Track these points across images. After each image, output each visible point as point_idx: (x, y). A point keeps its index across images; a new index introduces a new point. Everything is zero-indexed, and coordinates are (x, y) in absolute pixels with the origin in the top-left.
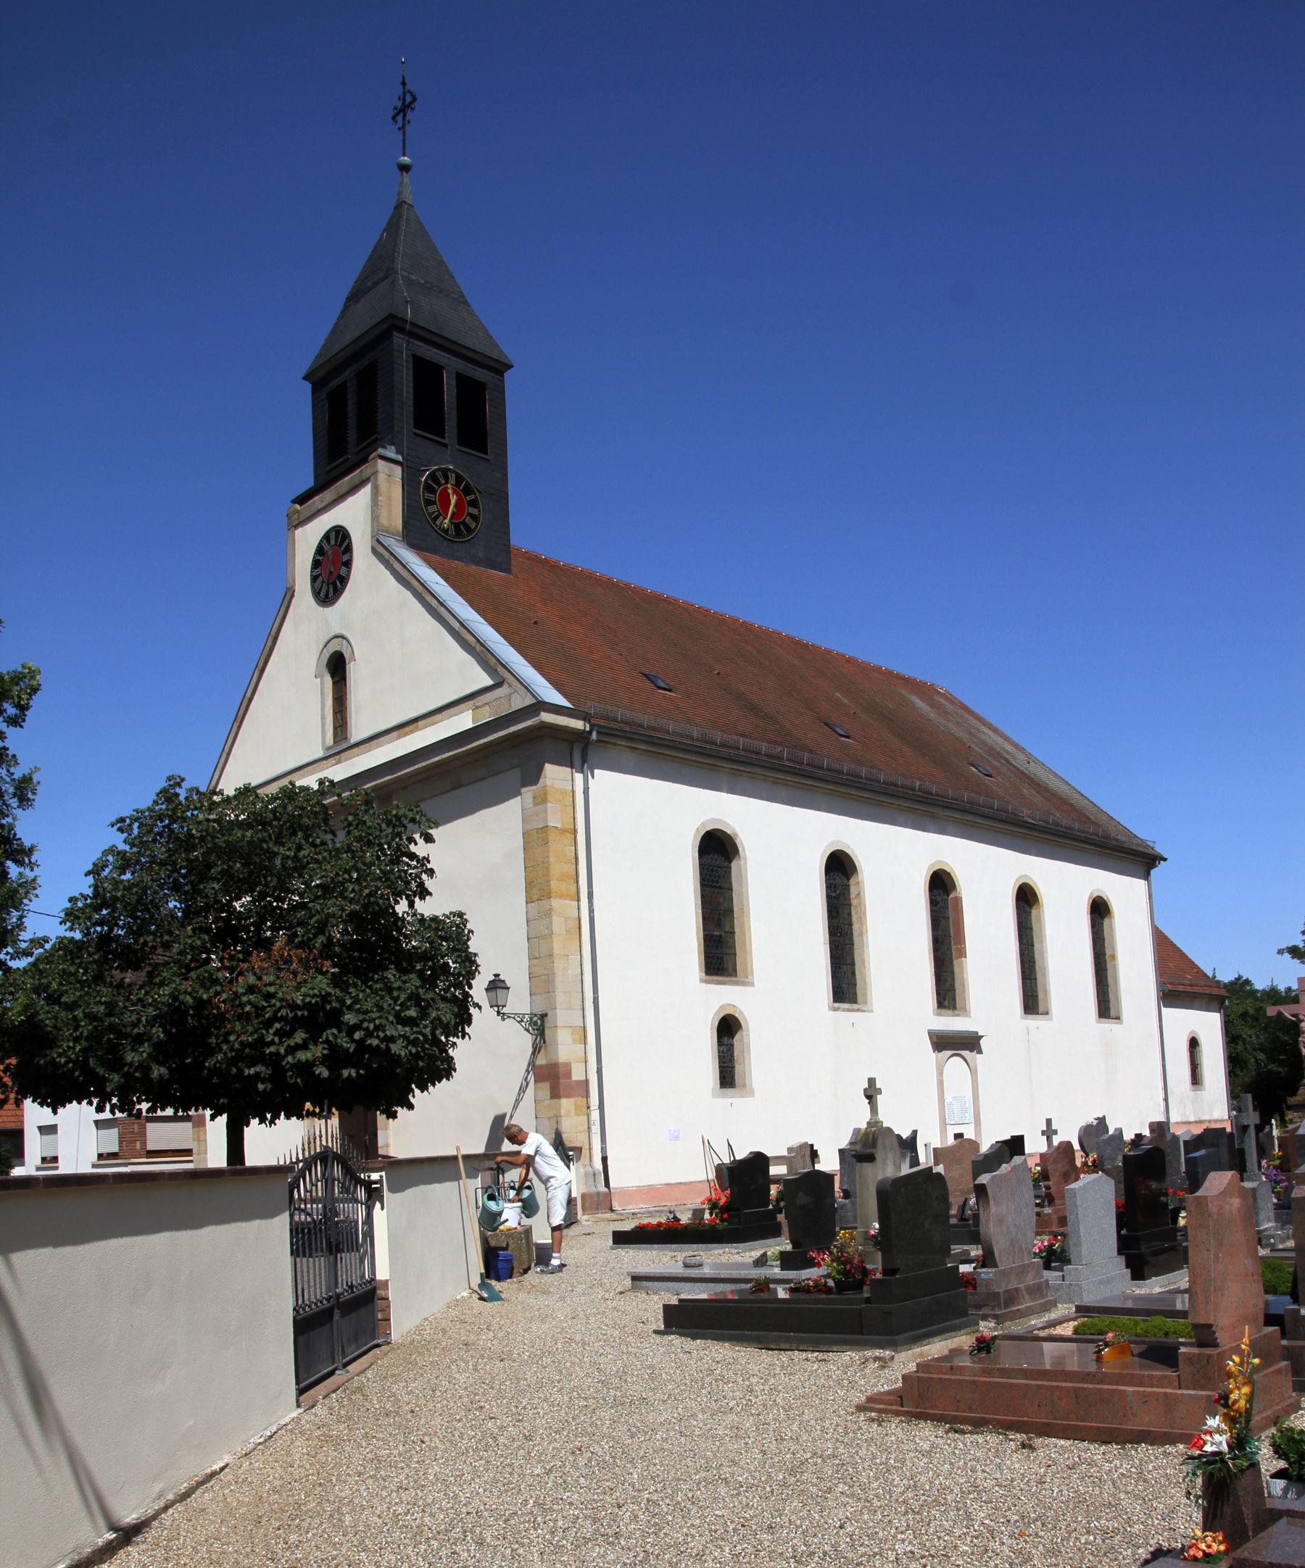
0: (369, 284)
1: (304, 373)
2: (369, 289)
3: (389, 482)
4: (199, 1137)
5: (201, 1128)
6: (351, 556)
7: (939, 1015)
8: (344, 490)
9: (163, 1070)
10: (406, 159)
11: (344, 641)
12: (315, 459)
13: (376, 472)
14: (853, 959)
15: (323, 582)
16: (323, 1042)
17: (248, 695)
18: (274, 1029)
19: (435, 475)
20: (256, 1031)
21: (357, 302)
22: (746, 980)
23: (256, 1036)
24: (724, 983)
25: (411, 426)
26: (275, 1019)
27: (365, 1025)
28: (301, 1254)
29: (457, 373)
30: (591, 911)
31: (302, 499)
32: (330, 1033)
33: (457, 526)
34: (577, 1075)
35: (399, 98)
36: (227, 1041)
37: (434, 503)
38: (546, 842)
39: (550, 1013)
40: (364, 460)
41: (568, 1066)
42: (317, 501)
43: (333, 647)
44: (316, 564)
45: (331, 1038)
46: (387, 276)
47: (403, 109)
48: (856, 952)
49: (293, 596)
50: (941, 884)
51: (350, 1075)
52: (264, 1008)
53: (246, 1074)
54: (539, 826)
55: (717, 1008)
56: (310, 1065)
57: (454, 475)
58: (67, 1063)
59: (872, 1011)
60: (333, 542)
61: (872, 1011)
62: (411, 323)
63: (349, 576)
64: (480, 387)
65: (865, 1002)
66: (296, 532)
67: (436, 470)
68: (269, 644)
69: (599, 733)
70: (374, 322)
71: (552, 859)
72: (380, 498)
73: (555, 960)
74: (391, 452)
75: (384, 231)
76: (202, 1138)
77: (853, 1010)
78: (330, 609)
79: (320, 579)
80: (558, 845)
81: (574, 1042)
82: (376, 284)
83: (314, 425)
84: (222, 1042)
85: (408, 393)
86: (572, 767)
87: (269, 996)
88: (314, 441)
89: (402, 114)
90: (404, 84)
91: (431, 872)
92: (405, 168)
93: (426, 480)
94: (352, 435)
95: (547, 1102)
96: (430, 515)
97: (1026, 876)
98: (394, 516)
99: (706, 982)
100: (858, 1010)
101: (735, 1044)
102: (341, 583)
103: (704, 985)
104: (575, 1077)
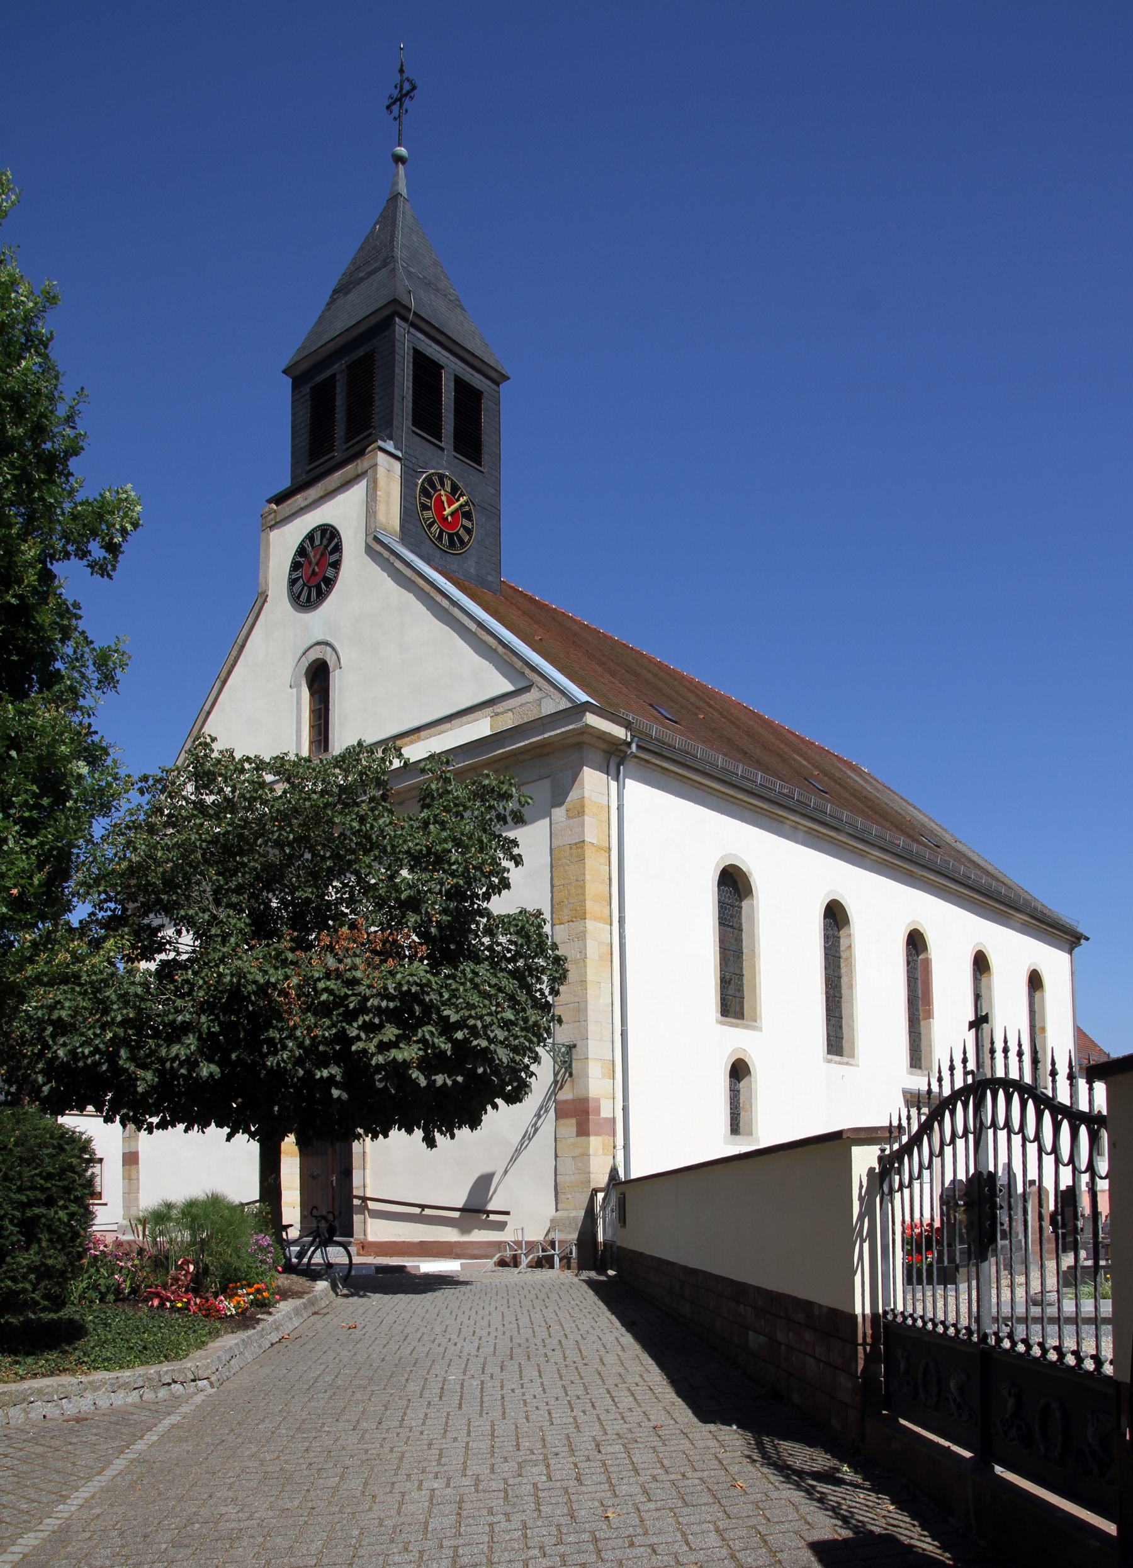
0: (361, 275)
1: (284, 366)
2: (361, 280)
3: (387, 477)
4: (130, 1175)
5: (133, 1167)
6: (341, 557)
7: (912, 1074)
8: (333, 486)
9: (214, 1068)
10: (402, 151)
11: (328, 648)
12: (293, 458)
13: (376, 465)
14: (841, 1012)
15: (304, 585)
16: (417, 1042)
17: (207, 708)
18: (360, 1022)
19: (431, 479)
20: (334, 1025)
21: (347, 294)
22: (755, 1024)
23: (334, 1031)
24: (736, 1026)
25: (410, 424)
26: (362, 1009)
27: (471, 1022)
28: (915, 1280)
29: (455, 375)
30: (622, 937)
31: (279, 499)
32: (426, 1031)
33: (451, 536)
34: (605, 1113)
35: (396, 87)
36: (291, 1036)
37: (429, 508)
38: (582, 859)
39: (579, 1044)
40: (361, 453)
41: (598, 1100)
42: (299, 500)
43: (315, 654)
44: (295, 566)
45: (428, 1037)
46: (385, 264)
47: (401, 97)
48: (844, 1005)
49: (265, 601)
50: (916, 942)
51: (445, 1083)
52: (347, 996)
53: (318, 1077)
54: (574, 842)
55: (730, 1051)
56: (406, 1065)
57: (449, 482)
58: (92, 1054)
59: (858, 1066)
60: (317, 542)
61: (858, 1066)
62: (415, 314)
63: (336, 577)
64: (477, 395)
65: (852, 1056)
66: (272, 534)
67: (432, 474)
68: (234, 653)
69: (638, 747)
70: (373, 309)
71: (588, 877)
72: (379, 493)
73: (589, 987)
74: (389, 446)
75: (376, 224)
76: (134, 1176)
77: (842, 1064)
78: (313, 614)
79: (301, 582)
80: (593, 864)
81: (604, 1076)
82: (370, 274)
83: (293, 421)
84: (286, 1038)
85: (408, 388)
86: (608, 774)
87: (353, 983)
88: (293, 439)
89: (398, 103)
90: (401, 71)
91: (518, 860)
92: (399, 159)
93: (423, 483)
94: (340, 431)
95: (572, 1140)
96: (426, 520)
97: (981, 943)
98: (390, 514)
99: (721, 1023)
100: (847, 1064)
101: (742, 1091)
102: (327, 586)
103: (719, 1026)
104: (603, 1115)
